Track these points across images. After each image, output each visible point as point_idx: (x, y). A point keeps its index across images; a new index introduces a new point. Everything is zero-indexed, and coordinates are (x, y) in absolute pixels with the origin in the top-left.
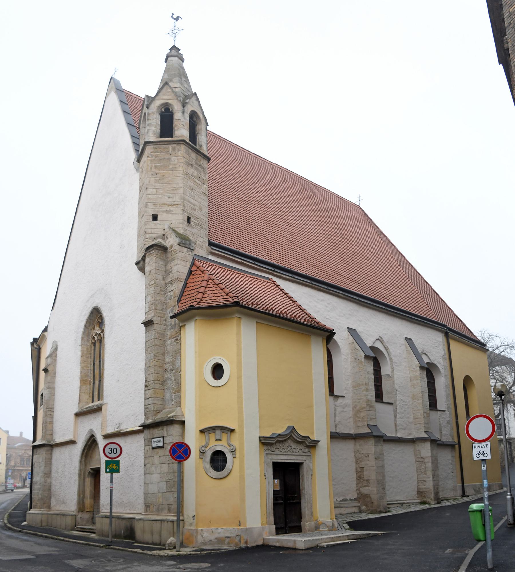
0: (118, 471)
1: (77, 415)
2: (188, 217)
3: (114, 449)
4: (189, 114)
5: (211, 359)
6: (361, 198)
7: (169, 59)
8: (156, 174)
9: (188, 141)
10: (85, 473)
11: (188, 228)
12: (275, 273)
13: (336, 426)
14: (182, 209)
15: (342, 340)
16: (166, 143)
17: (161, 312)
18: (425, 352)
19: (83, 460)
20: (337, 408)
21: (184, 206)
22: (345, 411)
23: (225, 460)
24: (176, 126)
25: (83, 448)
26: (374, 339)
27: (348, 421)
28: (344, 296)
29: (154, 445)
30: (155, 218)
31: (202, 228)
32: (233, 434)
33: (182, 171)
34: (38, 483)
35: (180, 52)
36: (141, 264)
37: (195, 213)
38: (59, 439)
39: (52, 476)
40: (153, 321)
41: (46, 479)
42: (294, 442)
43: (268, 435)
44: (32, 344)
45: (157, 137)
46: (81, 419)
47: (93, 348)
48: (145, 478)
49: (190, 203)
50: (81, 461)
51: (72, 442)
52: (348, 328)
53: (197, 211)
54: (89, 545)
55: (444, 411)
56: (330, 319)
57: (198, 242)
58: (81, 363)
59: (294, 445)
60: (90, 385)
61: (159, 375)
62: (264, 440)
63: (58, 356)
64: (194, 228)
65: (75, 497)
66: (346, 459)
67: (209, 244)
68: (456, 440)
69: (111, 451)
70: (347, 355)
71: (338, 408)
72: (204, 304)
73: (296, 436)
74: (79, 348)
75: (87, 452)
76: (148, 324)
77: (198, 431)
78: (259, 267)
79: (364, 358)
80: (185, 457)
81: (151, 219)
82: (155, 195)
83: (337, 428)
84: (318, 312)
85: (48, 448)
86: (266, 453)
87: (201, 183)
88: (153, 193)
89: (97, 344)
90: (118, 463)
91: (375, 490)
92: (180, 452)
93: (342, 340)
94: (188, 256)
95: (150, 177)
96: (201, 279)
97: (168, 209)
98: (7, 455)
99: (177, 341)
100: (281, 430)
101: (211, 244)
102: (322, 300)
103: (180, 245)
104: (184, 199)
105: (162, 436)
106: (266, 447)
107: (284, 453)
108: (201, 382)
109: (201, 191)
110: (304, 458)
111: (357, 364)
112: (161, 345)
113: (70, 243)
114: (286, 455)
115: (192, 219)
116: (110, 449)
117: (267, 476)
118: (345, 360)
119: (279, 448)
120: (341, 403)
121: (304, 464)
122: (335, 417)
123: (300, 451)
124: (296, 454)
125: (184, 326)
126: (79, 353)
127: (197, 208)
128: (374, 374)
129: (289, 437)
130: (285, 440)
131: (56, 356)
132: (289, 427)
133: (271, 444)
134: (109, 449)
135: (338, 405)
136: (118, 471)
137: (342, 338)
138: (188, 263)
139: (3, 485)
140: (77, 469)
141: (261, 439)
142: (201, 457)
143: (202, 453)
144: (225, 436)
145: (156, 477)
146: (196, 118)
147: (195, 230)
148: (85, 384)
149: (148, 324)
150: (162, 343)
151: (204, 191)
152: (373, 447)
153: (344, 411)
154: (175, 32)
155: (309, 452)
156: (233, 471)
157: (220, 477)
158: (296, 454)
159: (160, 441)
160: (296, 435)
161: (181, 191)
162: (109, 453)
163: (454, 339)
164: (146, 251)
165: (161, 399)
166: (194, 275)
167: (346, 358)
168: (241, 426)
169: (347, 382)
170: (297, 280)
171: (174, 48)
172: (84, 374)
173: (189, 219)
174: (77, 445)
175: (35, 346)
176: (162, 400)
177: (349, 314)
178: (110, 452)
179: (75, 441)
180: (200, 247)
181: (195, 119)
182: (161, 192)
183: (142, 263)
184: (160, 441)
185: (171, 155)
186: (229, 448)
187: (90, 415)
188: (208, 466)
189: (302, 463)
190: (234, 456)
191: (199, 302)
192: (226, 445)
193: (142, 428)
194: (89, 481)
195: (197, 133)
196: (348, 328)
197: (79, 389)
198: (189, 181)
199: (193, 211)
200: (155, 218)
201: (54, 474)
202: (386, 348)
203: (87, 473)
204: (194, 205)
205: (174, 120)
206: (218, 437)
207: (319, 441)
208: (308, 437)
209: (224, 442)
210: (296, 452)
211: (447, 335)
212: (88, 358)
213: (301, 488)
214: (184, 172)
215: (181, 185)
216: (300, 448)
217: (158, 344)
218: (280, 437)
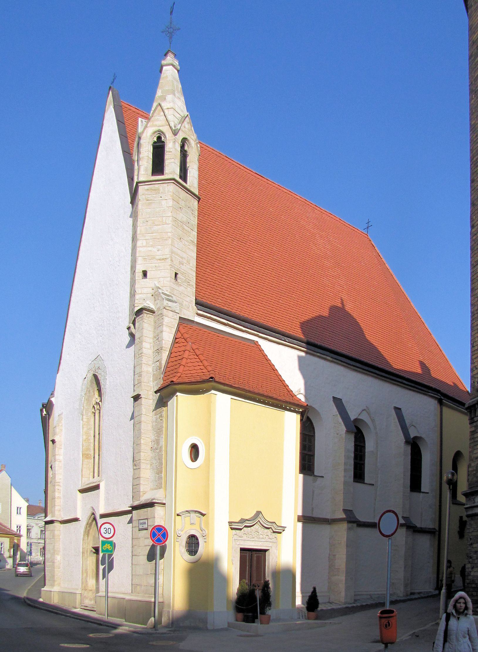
2: (175, 273)
3: (108, 529)
6: (370, 224)
8: (147, 221)
9: (178, 178)
11: (176, 287)
14: (170, 264)
18: (414, 424)
21: (172, 260)
26: (360, 410)
29: (141, 527)
31: (189, 285)
53: (185, 264)
54: (52, 609)
55: (428, 493)
57: (185, 303)
68: (437, 529)
80: (163, 540)
87: (189, 230)
89: (97, 412)
92: (159, 535)
96: (183, 348)
97: (157, 265)
104: (172, 252)
107: (252, 539)
109: (190, 240)
110: (271, 544)
116: (105, 529)
121: (270, 551)
134: (104, 528)
138: (173, 329)
148: (87, 458)
158: (263, 540)
159: (145, 523)
160: (263, 520)
161: (170, 242)
162: (104, 533)
163: (450, 407)
172: (86, 447)
173: (176, 274)
179: (79, 519)
182: (151, 243)
184: (145, 523)
185: (161, 197)
186: (201, 532)
187: (337, 351)
190: (205, 540)
193: (131, 508)
196: (334, 398)
198: (177, 229)
199: (181, 265)
202: (373, 421)
204: (182, 258)
211: (440, 402)
215: (170, 234)
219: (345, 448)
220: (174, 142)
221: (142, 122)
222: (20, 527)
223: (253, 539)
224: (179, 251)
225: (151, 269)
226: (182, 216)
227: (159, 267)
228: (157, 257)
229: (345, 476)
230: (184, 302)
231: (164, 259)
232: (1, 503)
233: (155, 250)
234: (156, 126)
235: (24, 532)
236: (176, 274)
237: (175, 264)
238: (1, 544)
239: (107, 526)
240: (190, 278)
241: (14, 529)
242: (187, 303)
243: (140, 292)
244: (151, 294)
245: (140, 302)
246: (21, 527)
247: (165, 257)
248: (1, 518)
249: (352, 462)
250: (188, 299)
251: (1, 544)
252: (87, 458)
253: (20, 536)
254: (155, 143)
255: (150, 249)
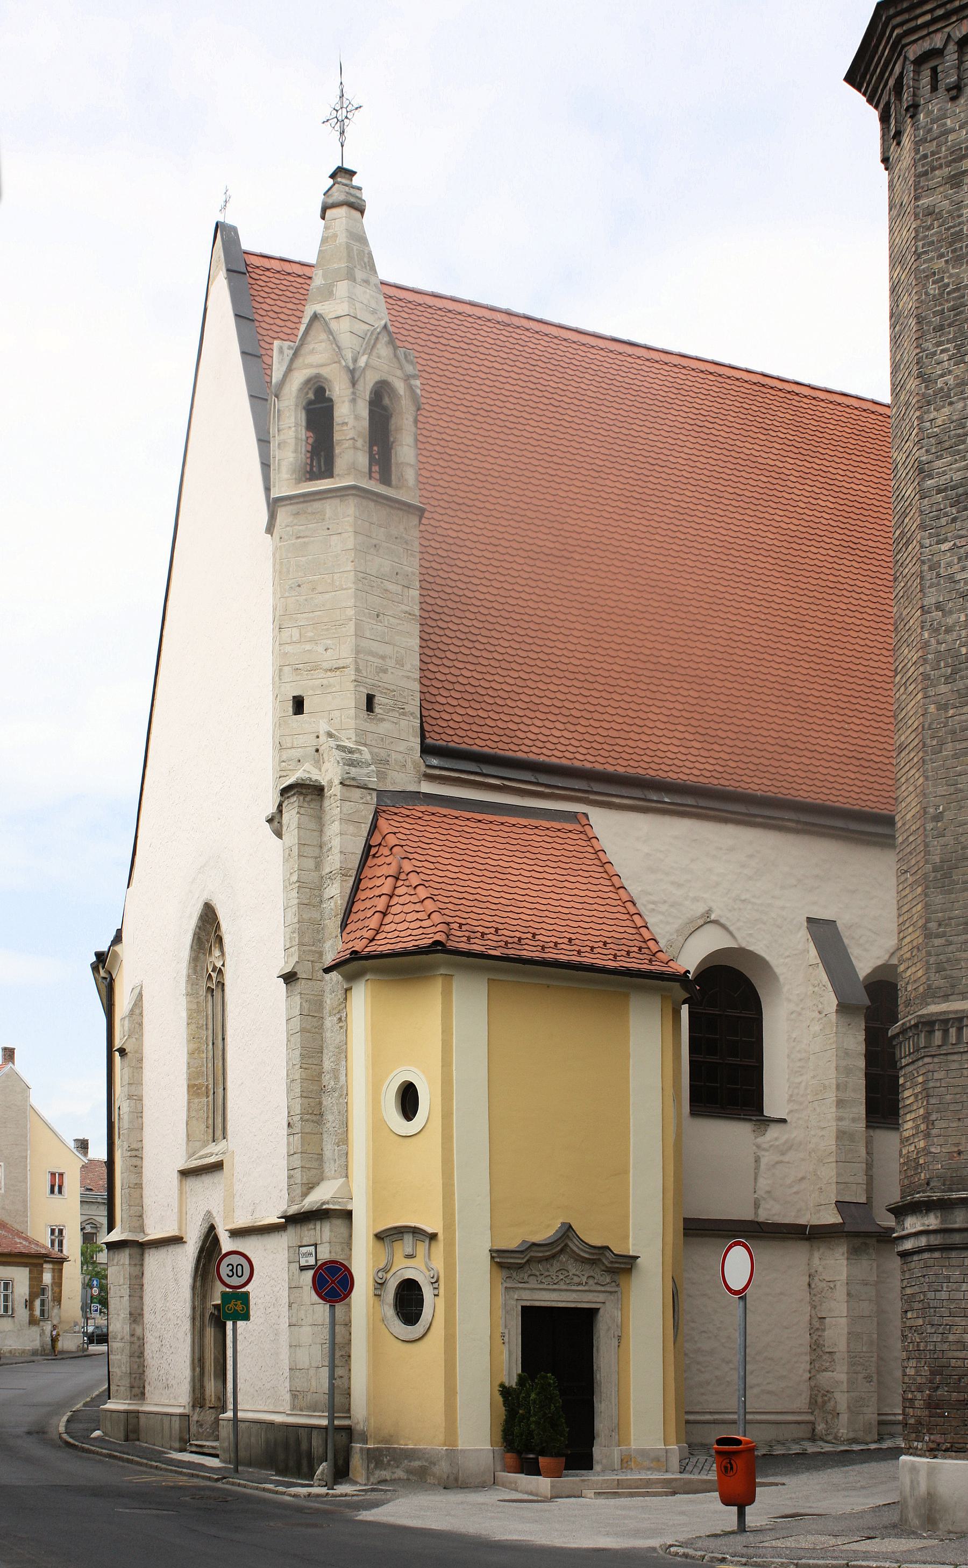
0: (246, 1317)
1: (185, 1174)
4: (368, 398)
5: (393, 1075)
7: (328, 212)
8: (299, 586)
9: (365, 484)
10: (202, 1315)
12: (592, 797)
13: (757, 1206)
14: (353, 678)
15: (788, 956)
16: (317, 497)
17: (313, 948)
19: (198, 1284)
20: (761, 1153)
22: (788, 1163)
23: (420, 1302)
24: (339, 441)
25: (196, 1255)
27: (795, 1190)
28: (800, 827)
29: (303, 1263)
30: (298, 705)
31: (404, 714)
32: (433, 1244)
33: (353, 573)
34: (119, 1337)
35: (356, 181)
36: (275, 821)
37: (386, 677)
38: (154, 1233)
39: (146, 1321)
40: (295, 974)
41: (133, 1326)
42: (576, 1260)
43: (513, 1244)
44: (95, 968)
45: (299, 481)
46: (194, 1184)
47: (210, 1003)
48: (291, 1333)
49: (374, 656)
50: (194, 1288)
51: (177, 1240)
52: (809, 920)
53: (390, 670)
56: (753, 900)
57: (394, 756)
58: (189, 1041)
59: (573, 1268)
60: (208, 1097)
61: (311, 1100)
62: (499, 1257)
63: (145, 1013)
64: (382, 720)
65: (187, 1373)
66: (781, 1294)
67: (422, 752)
69: (232, 1270)
70: (801, 1000)
71: (767, 1154)
72: (382, 946)
73: (578, 1248)
74: (183, 1001)
75: (204, 1265)
76: (289, 978)
77: (371, 1237)
78: (547, 790)
79: (837, 1011)
81: (291, 710)
82: (298, 645)
83: (761, 1211)
84: (717, 884)
85: (136, 1251)
86: (505, 1285)
88: (294, 639)
90: (245, 1297)
91: (843, 1377)
92: (333, 1282)
93: (788, 956)
94: (362, 807)
95: (287, 594)
97: (325, 682)
98: (82, 1229)
99: (341, 1024)
100: (544, 1232)
101: (427, 750)
102: (731, 849)
103: (344, 785)
105: (312, 1242)
106: (505, 1273)
107: (550, 1287)
108: (378, 1126)
110: (601, 1297)
111: (821, 1027)
112: (314, 1030)
113: (156, 702)
114: (554, 1290)
115: (377, 700)
116: (230, 1267)
117: (506, 1339)
118: (793, 1016)
119: (538, 1273)
120: (776, 1139)
121: (601, 1311)
122: (756, 1179)
123: (591, 1282)
124: (580, 1288)
125: (350, 989)
126: (184, 1014)
127: (391, 663)
128: (865, 1056)
129: (559, 1248)
130: (553, 1256)
131: (141, 1014)
132: (563, 1224)
133: (520, 1267)
135: (765, 1146)
136: (246, 1317)
137: (787, 954)
139: (77, 1329)
140: (188, 1305)
141: (494, 1255)
142: (378, 1292)
143: (380, 1285)
144: (422, 1248)
145: (306, 1333)
146: (389, 396)
147: (386, 725)
149: (289, 978)
150: (316, 1024)
151: (407, 609)
152: (845, 1262)
153: (781, 1162)
154: (342, 114)
155: (613, 1284)
156: (434, 1324)
157: (411, 1337)
158: (580, 1288)
164: (282, 795)
165: (316, 1156)
166: (374, 856)
167: (798, 1009)
168: (449, 1225)
169: (798, 1080)
170: (654, 805)
171: (342, 173)
173: (370, 699)
174: (186, 1246)
175: (102, 971)
176: (317, 1159)
177: (817, 876)
178: (231, 1274)
180: (397, 768)
181: (386, 401)
182: (310, 634)
183: (277, 817)
186: (428, 1273)
188: (390, 1312)
189: (598, 1309)
191: (373, 939)
192: (423, 1268)
193: (283, 1220)
194: (210, 1333)
195: (392, 439)
196: (809, 920)
197: (185, 1109)
200: (298, 705)
201: (148, 1317)
203: (207, 1316)
204: (383, 658)
205: (336, 428)
206: (409, 1250)
207: (638, 1257)
208: (607, 1248)
209: (418, 1262)
210: (579, 1284)
212: (201, 1028)
213: (595, 1368)
214: (356, 576)
216: (592, 1274)
217: (308, 1027)
218: (535, 1248)
219: (837, 1049)
220: (354, 401)
221: (281, 351)
222: (61, 1231)
223: (555, 1287)
224: (375, 644)
225: (311, 692)
226: (381, 564)
227: (329, 686)
228: (326, 665)
229: (840, 1119)
230: (393, 754)
231: (338, 668)
232: (2, 1164)
233: (320, 649)
234: (312, 366)
235: (73, 1246)
236: (370, 699)
237: (365, 675)
238: (6, 1286)
239: (235, 1259)
240: (404, 697)
241: (45, 1240)
242: (400, 757)
243: (289, 745)
244: (314, 749)
245: (290, 767)
246: (64, 1232)
247: (341, 663)
248: (3, 1208)
249: (859, 1082)
250: (402, 747)
251: (6, 1286)
252: (198, 1094)
253: (59, 1262)
254: (310, 403)
255: (308, 647)
